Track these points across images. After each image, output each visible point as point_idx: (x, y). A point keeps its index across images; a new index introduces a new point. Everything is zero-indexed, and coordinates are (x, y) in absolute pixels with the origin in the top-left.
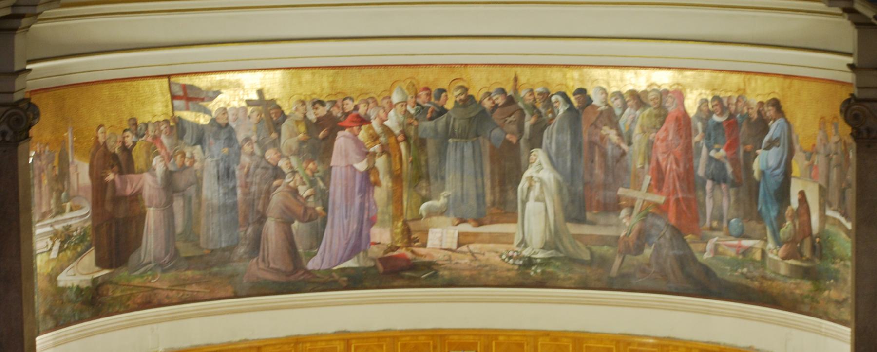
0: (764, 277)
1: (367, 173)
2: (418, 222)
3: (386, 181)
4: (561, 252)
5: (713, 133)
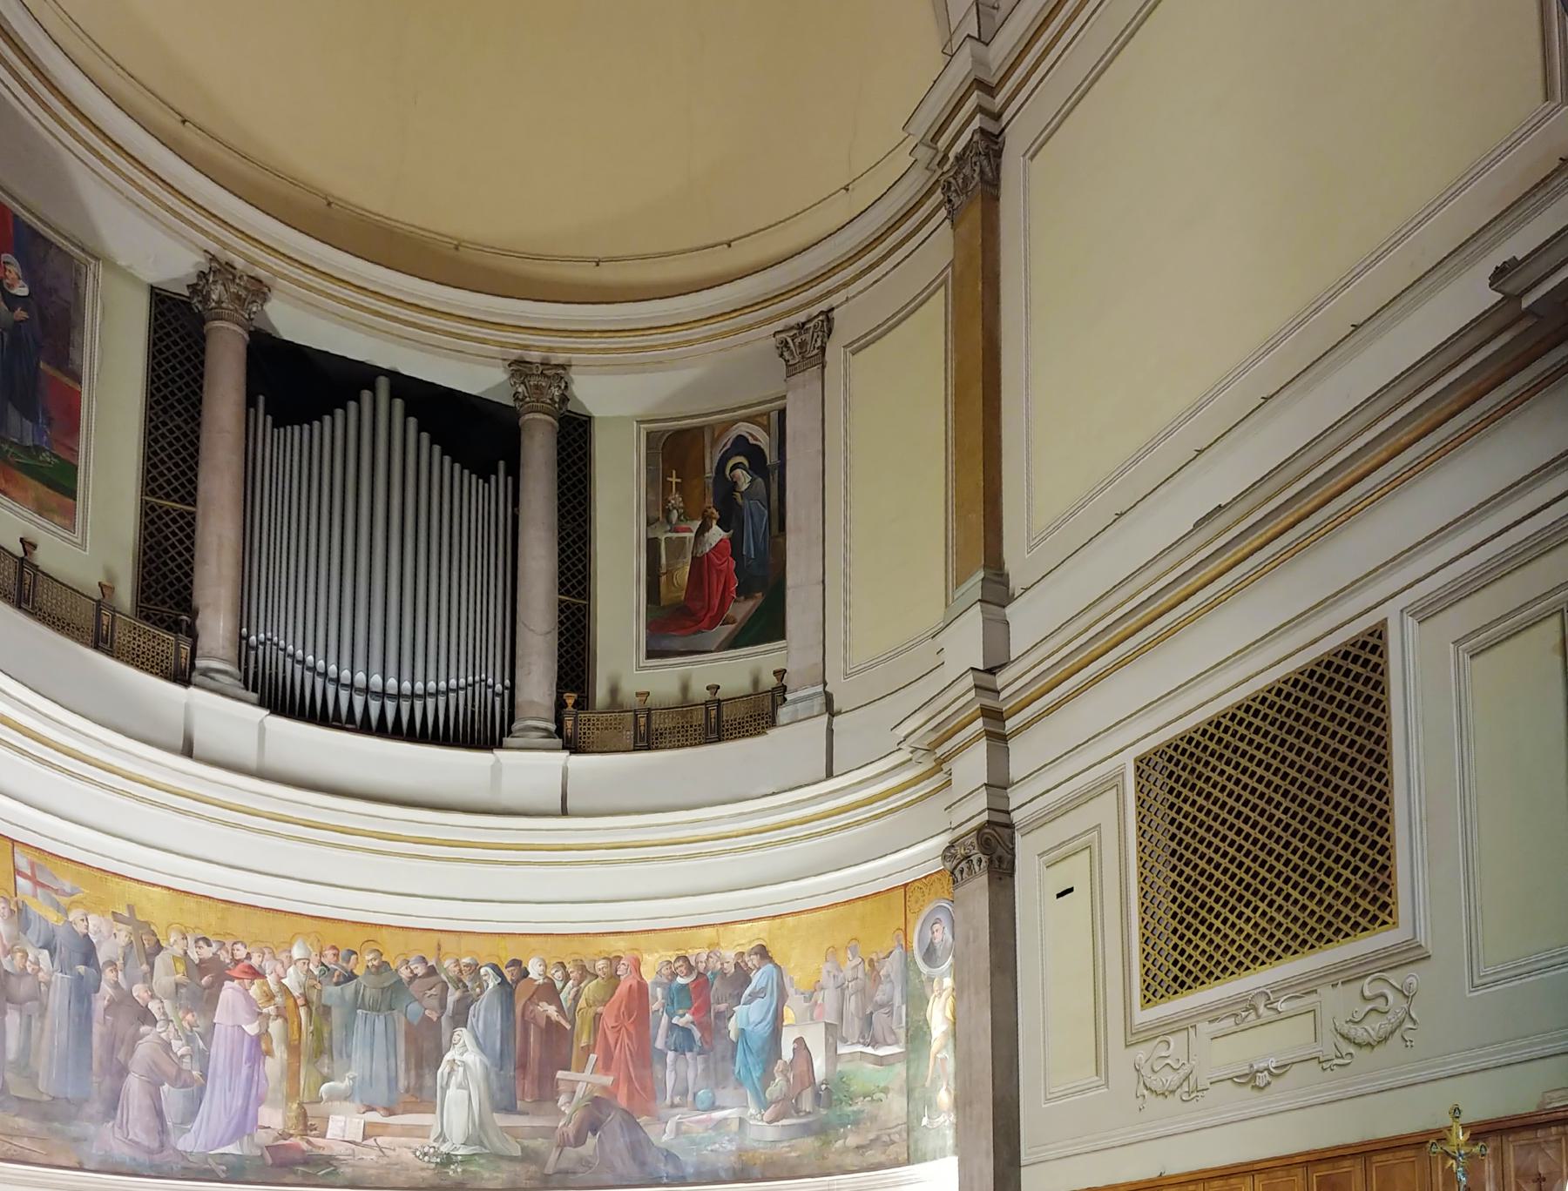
1: (257, 1040)
2: (317, 1105)
3: (280, 1052)
4: (485, 1148)
5: (678, 998)
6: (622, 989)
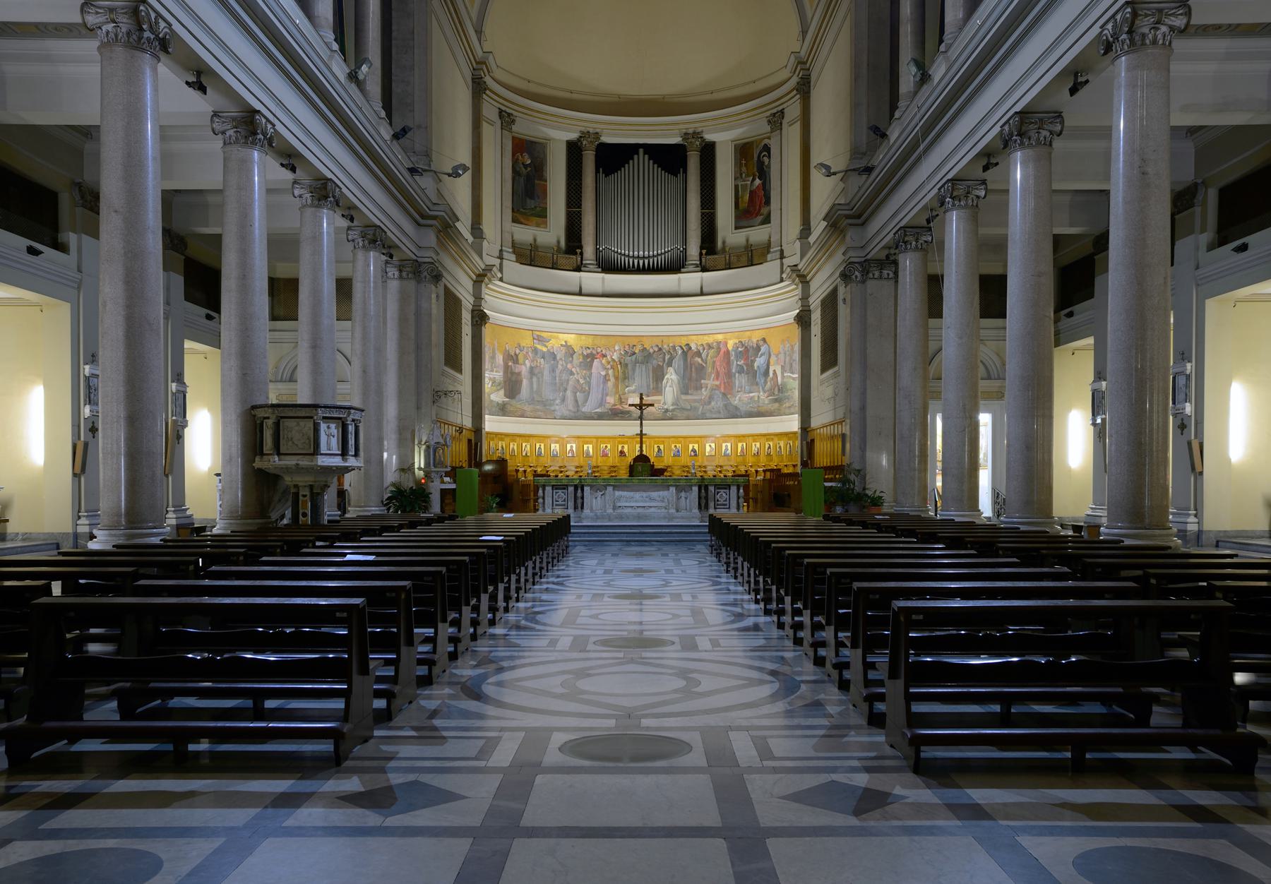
0: (759, 406)
3: (612, 379)
5: (739, 355)
6: (722, 353)
